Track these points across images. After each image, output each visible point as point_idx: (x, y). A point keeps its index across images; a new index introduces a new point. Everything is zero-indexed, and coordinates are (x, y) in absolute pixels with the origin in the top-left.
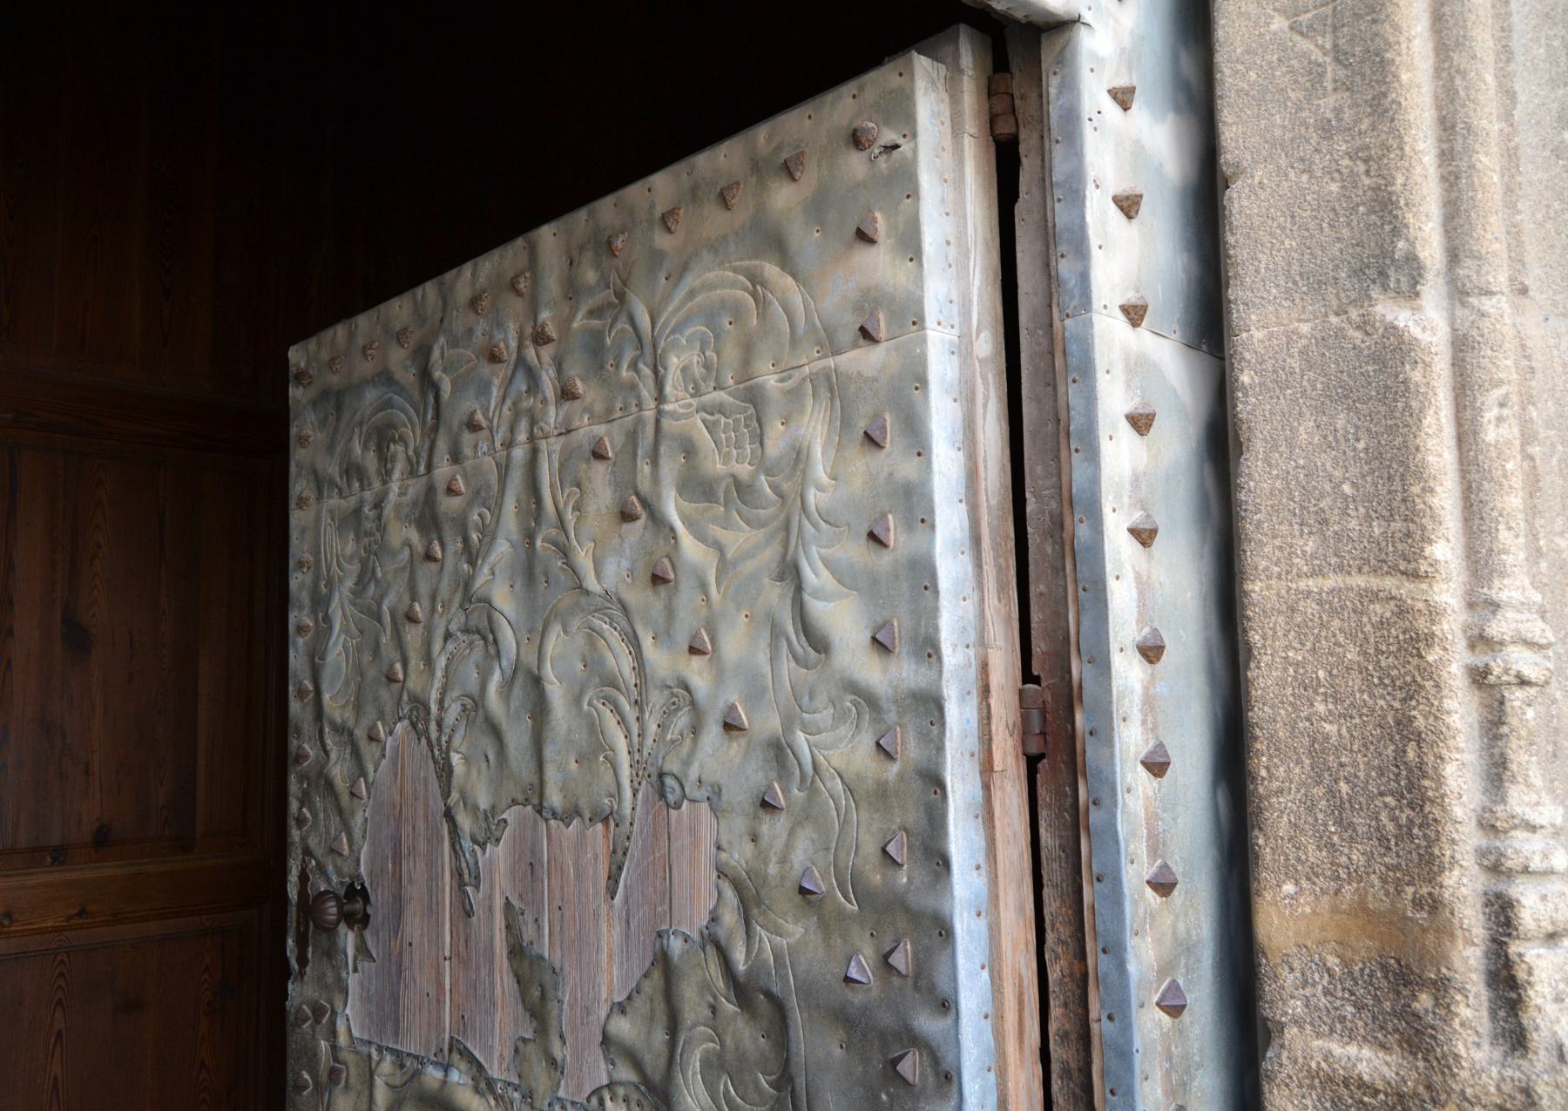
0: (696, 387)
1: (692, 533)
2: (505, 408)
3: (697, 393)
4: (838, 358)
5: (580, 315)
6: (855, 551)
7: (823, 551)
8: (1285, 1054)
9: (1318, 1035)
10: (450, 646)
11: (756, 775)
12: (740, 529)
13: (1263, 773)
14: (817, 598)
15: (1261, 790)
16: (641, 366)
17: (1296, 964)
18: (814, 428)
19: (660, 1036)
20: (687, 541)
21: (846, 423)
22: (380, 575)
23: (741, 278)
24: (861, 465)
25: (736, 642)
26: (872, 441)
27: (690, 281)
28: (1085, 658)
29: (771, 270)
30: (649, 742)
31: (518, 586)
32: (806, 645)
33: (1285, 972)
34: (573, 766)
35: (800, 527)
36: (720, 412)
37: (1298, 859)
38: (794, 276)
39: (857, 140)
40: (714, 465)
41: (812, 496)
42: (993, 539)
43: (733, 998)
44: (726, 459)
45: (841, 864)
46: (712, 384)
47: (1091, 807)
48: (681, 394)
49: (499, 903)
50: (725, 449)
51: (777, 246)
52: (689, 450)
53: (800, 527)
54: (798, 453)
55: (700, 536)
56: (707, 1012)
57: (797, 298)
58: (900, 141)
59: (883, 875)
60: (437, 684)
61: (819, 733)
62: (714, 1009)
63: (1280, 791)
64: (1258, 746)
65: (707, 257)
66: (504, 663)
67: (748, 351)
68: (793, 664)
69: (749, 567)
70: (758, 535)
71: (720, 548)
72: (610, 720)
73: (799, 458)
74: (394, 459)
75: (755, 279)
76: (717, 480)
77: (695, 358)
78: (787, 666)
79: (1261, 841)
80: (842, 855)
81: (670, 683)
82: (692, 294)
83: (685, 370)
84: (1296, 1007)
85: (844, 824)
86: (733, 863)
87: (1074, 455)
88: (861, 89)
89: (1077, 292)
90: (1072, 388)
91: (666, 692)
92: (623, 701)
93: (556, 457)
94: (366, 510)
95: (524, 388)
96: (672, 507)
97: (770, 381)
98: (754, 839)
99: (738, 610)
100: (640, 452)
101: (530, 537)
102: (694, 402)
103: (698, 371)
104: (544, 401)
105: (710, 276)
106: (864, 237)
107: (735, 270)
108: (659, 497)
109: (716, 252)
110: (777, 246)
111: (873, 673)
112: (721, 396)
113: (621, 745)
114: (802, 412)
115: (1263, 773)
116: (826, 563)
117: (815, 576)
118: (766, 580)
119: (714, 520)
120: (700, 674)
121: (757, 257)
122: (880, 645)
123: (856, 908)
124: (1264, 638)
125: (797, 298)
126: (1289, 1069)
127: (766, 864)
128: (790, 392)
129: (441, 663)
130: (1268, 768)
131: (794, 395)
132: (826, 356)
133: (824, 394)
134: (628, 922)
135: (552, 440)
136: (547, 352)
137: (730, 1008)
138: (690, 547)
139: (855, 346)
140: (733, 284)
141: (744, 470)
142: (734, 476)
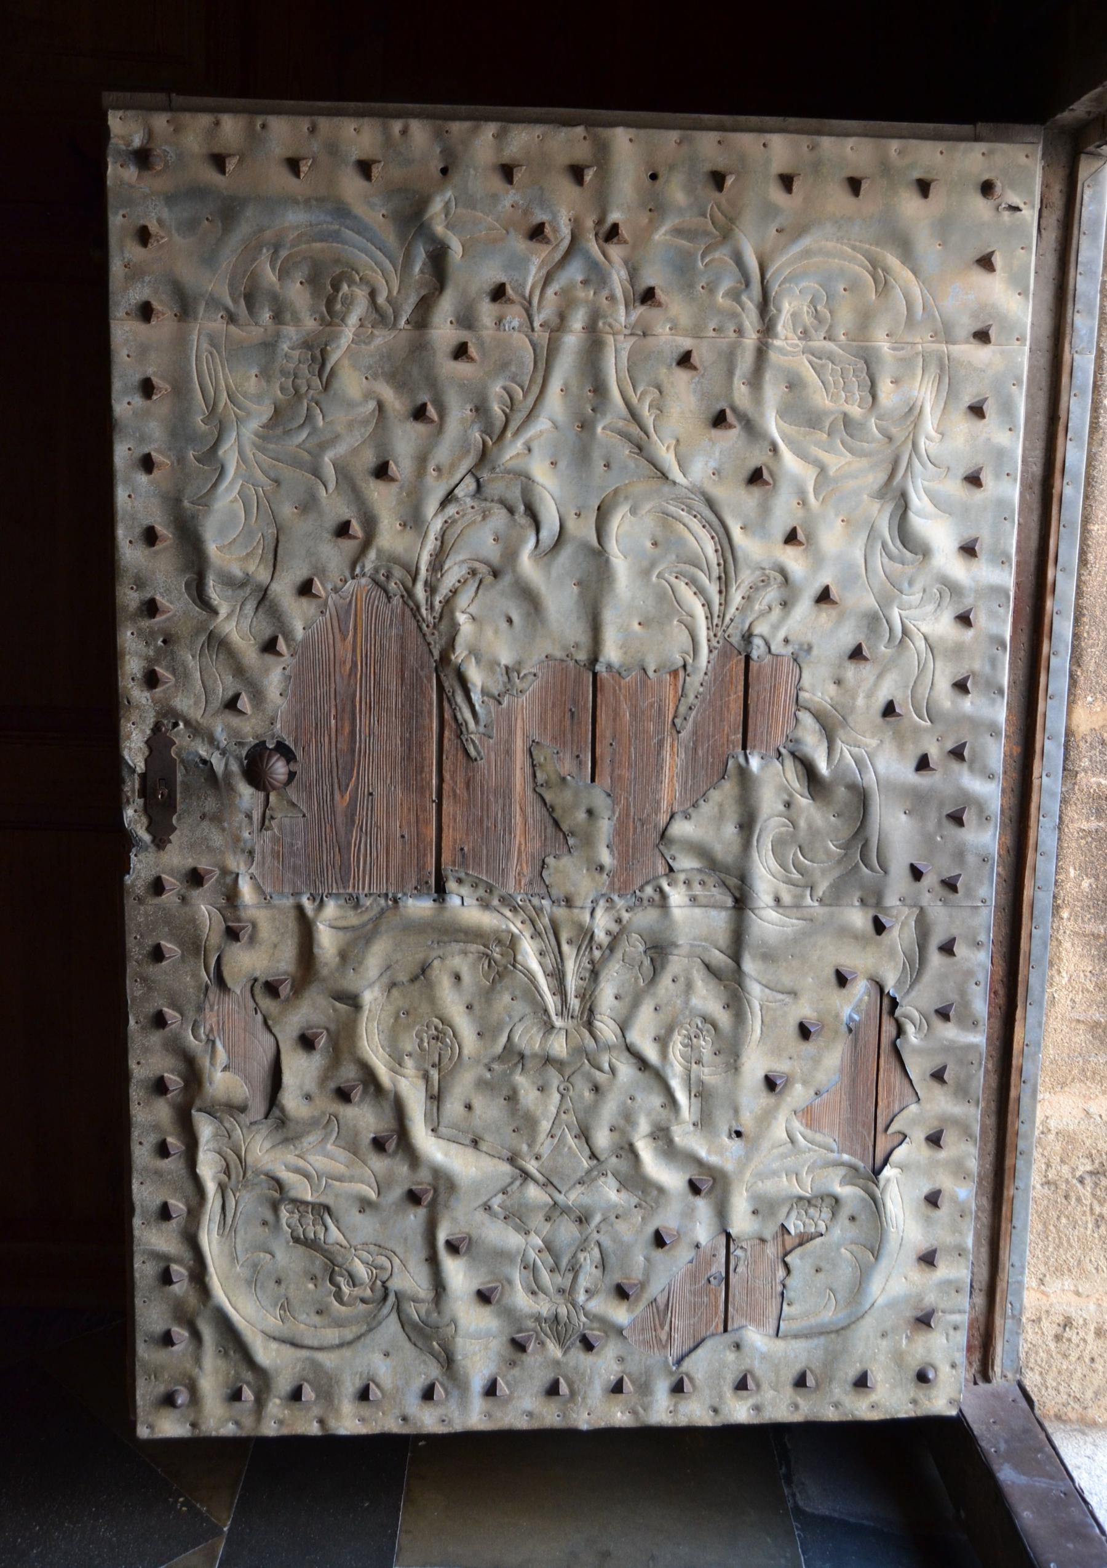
0: (805, 332)
1: (791, 450)
2: (550, 292)
3: (805, 334)
4: (951, 347)
5: (663, 230)
6: (954, 488)
7: (926, 483)
8: (1077, 787)
9: (1094, 775)
10: (451, 510)
11: (848, 636)
12: (842, 455)
13: (1085, 635)
14: (919, 516)
15: (1083, 644)
16: (744, 298)
17: (1089, 740)
18: (925, 392)
19: (730, 830)
20: (788, 456)
21: (952, 394)
22: (320, 422)
23: (859, 256)
24: (962, 427)
25: (832, 537)
26: (977, 411)
27: (806, 242)
28: (1059, 568)
29: (893, 261)
30: (732, 611)
31: (562, 464)
32: (901, 547)
33: (1082, 744)
34: (636, 627)
35: (910, 463)
36: (829, 358)
37: (1097, 683)
38: (915, 273)
39: (987, 188)
40: (821, 399)
41: (922, 444)
42: (192, 379)
43: (807, 794)
44: (834, 398)
45: (919, 696)
46: (823, 335)
47: (1052, 656)
48: (790, 335)
49: (519, 746)
50: (832, 390)
51: (905, 248)
52: (794, 384)
53: (910, 463)
54: (911, 409)
55: (801, 453)
56: (781, 807)
57: (916, 291)
58: (1022, 206)
59: (952, 702)
60: (431, 544)
61: (910, 608)
62: (788, 805)
63: (1093, 646)
64: (1085, 619)
65: (829, 228)
66: (544, 534)
67: (865, 320)
68: (886, 560)
69: (851, 484)
70: (861, 463)
71: (822, 469)
72: (687, 593)
73: (912, 414)
74: (348, 302)
75: (875, 265)
76: (827, 413)
77: (805, 309)
78: (879, 560)
79: (1079, 673)
80: (920, 690)
81: (765, 565)
82: (807, 253)
83: (795, 316)
84: (1085, 763)
85: (922, 670)
86: (817, 699)
87: (1068, 442)
88: (991, 152)
89: (1086, 339)
90: (1073, 400)
91: (758, 573)
92: (703, 578)
93: (624, 355)
94: (285, 347)
95: (580, 278)
96: (773, 425)
97: (884, 346)
98: (838, 682)
99: (837, 515)
100: (738, 373)
101: (585, 426)
102: (801, 344)
103: (808, 319)
104: (612, 298)
105: (830, 245)
106: (986, 263)
107: (854, 248)
108: (762, 415)
109: (840, 228)
110: (905, 248)
111: (957, 569)
112: (830, 346)
113: (700, 612)
114: (913, 376)
115: (1085, 635)
116: (927, 492)
117: (918, 501)
118: (865, 496)
119: (818, 444)
120: (796, 561)
121: (877, 245)
122: (969, 550)
123: (929, 723)
124: (1095, 557)
125: (916, 291)
126: (1078, 795)
127: (854, 698)
128: (901, 360)
129: (436, 526)
130: (1088, 633)
131: (907, 363)
132: (940, 342)
133: (933, 370)
134: (695, 749)
135: (621, 338)
136: (616, 252)
137: (803, 801)
138: (789, 460)
139: (967, 342)
140: (852, 260)
141: (855, 411)
142: (845, 415)
